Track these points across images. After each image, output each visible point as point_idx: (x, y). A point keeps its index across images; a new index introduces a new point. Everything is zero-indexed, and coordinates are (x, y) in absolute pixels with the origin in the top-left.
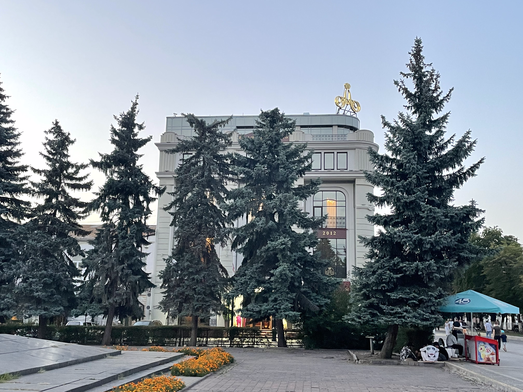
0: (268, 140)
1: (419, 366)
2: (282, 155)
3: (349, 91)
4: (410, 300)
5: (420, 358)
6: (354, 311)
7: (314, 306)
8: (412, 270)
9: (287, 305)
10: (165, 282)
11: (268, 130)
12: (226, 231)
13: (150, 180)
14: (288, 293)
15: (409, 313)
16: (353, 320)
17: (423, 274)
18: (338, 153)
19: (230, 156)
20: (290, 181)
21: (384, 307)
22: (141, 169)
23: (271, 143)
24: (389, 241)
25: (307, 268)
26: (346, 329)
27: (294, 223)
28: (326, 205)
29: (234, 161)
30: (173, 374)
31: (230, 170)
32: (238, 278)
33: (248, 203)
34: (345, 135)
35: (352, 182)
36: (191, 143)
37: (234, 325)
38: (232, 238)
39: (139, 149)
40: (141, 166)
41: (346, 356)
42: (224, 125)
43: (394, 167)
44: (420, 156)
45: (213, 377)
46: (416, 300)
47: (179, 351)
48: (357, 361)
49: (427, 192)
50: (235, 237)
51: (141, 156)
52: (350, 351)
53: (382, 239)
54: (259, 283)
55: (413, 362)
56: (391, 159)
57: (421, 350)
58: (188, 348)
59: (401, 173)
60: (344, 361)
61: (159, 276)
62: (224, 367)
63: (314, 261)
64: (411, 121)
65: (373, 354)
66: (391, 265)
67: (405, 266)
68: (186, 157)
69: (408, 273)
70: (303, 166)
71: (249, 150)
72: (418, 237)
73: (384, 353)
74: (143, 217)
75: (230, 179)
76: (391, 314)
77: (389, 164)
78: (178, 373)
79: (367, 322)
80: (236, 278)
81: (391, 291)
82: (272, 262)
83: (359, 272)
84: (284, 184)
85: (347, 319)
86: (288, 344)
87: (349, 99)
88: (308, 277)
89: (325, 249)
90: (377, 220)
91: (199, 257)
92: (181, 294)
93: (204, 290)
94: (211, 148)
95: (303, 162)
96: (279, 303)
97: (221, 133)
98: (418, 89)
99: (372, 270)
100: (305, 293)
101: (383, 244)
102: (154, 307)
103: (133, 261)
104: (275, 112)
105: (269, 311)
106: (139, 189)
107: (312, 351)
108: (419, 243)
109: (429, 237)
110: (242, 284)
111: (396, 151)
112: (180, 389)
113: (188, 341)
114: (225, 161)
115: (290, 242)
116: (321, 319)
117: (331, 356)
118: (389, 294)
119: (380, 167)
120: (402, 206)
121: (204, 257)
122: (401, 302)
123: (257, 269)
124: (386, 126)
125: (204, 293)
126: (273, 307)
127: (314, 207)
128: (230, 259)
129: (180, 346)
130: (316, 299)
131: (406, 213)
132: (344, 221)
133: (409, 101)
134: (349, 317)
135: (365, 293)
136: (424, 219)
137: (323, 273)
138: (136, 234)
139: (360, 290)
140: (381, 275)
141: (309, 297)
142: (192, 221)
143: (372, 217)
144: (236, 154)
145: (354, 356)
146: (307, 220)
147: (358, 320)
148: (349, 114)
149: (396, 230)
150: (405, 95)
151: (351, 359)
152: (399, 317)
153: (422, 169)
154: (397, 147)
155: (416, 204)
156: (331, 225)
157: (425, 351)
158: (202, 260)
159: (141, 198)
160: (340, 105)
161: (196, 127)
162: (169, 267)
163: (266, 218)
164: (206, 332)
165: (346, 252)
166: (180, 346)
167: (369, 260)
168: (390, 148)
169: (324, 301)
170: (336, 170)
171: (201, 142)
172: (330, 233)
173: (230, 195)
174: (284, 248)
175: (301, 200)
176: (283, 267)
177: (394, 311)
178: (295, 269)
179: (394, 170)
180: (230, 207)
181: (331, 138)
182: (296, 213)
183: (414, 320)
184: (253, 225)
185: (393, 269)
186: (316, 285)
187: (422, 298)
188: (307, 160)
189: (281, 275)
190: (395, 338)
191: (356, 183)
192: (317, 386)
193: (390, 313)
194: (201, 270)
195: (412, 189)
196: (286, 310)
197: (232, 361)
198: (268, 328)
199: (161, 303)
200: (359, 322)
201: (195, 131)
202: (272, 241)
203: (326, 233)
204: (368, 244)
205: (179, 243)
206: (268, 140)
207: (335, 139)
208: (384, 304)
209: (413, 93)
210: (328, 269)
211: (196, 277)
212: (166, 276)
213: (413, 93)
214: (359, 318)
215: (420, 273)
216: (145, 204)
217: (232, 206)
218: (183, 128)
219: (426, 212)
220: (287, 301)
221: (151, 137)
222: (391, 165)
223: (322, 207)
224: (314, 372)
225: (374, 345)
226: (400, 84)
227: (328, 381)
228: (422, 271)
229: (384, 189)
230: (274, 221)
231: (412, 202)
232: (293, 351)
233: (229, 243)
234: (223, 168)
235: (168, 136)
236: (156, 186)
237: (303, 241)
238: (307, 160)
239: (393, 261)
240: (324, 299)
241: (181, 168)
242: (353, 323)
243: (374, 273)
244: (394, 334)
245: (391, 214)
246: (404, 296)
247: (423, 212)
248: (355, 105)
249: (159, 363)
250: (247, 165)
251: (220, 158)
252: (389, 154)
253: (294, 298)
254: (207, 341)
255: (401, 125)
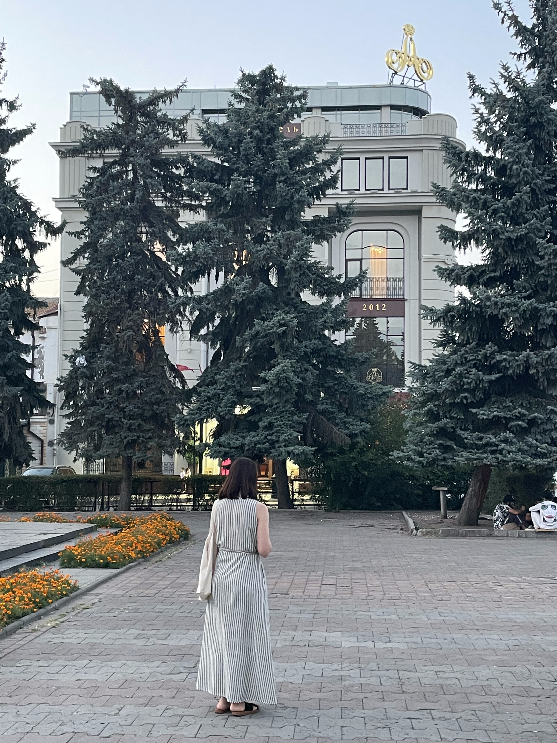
0: (254, 128)
1: (526, 537)
2: (282, 157)
3: (411, 39)
4: (513, 420)
5: (530, 523)
6: (411, 442)
7: (340, 435)
8: (519, 366)
9: (291, 435)
10: (68, 397)
11: (254, 108)
12: (178, 301)
13: (33, 209)
14: (293, 414)
15: (511, 443)
16: (409, 459)
17: (538, 372)
18: (390, 158)
19: (182, 160)
20: (296, 206)
21: (465, 434)
22: (16, 187)
23: (260, 134)
24: (476, 312)
25: (329, 368)
26: (395, 474)
27: (305, 287)
28: (366, 255)
29: (190, 170)
30: (64, 565)
31: (185, 188)
32: (203, 389)
33: (218, 249)
34: (404, 125)
35: (416, 212)
36: (107, 136)
37: (203, 473)
38: (191, 315)
39: (11, 149)
40: (15, 181)
41: (397, 523)
42: (171, 100)
43: (491, 173)
44: (538, 149)
45: (142, 567)
46: (523, 421)
47: (90, 521)
48: (415, 532)
49: (549, 219)
50: (197, 313)
51: (15, 162)
52: (404, 513)
53: (464, 309)
54: (241, 398)
55: (517, 532)
56: (485, 158)
57: (530, 509)
58: (104, 515)
59: (503, 182)
60: (392, 532)
61: (57, 385)
62: (168, 548)
63: (342, 355)
64: (523, 81)
65: (446, 517)
66: (480, 357)
67: (505, 360)
68: (99, 164)
69: (511, 371)
70: (322, 179)
71: (220, 149)
72: (531, 304)
73: (464, 517)
74: (25, 278)
75: (186, 207)
76: (478, 447)
77: (480, 169)
78: (73, 563)
79: (435, 460)
80: (199, 389)
81: (480, 404)
82: (264, 357)
83: (422, 373)
84: (286, 214)
85: (399, 458)
86: (296, 503)
87: (412, 54)
88: (331, 384)
89: (369, 336)
90: (454, 275)
91: (131, 352)
92: (98, 418)
93: (140, 411)
94: (147, 144)
95: (322, 172)
96: (277, 432)
97: (165, 115)
98: (538, 19)
99: (445, 367)
100: (324, 412)
101: (466, 319)
102: (52, 444)
103: (6, 360)
104: (268, 73)
105: (258, 446)
106: (13, 226)
107: (337, 515)
108: (534, 316)
109: (552, 304)
110: (209, 399)
111: (494, 141)
112: (66, 595)
113: (116, 502)
114: (174, 170)
115: (295, 321)
116: (353, 458)
117: (370, 522)
118: (474, 411)
119: (462, 175)
120: (503, 248)
121: (139, 351)
122: (496, 424)
123: (236, 371)
124: (476, 95)
125: (141, 416)
126: (266, 438)
127: (347, 261)
128: (187, 352)
129: (102, 509)
130: (345, 423)
131: (509, 260)
132: (401, 284)
133: (522, 41)
134: (401, 454)
135: (430, 410)
136: (543, 271)
137: (361, 378)
138: (10, 310)
139: (423, 404)
140: (461, 376)
141: (331, 418)
142: (114, 285)
143: (446, 270)
144: (195, 157)
145: (411, 522)
146: (331, 281)
147: (418, 459)
148: (411, 84)
149: (491, 293)
150: (513, 30)
151: (405, 529)
152: (493, 452)
153: (543, 175)
154: (495, 132)
155: (528, 243)
156: (378, 292)
157: (539, 512)
158: (138, 357)
159: (19, 243)
160: (395, 66)
161: (117, 104)
162: (75, 369)
163: (254, 277)
164: (149, 484)
165: (403, 339)
166: (102, 509)
167: (440, 350)
168: (482, 136)
169: (358, 427)
170: (386, 190)
171: (127, 133)
172: (375, 307)
173: (186, 236)
174: (284, 332)
175: (317, 243)
176: (283, 365)
177: (484, 441)
178: (307, 370)
179: (490, 178)
180: (185, 257)
181: (378, 130)
182: (309, 267)
183: (519, 457)
184: (227, 290)
185: (483, 365)
186: (344, 399)
187: (535, 417)
188: (329, 168)
189: (279, 381)
190: (485, 489)
191: (424, 215)
192: (332, 581)
193: (476, 445)
194: (135, 374)
195: (522, 214)
196: (288, 443)
197: (185, 536)
198: (266, 476)
199: (62, 435)
200: (420, 462)
201: (116, 112)
202: (263, 319)
203: (368, 308)
204: (438, 320)
205: (91, 325)
206: (254, 128)
207: (385, 132)
208: (465, 430)
209: (530, 27)
210: (371, 371)
211: (124, 387)
212: (68, 386)
213: (530, 27)
214: (421, 454)
215: (532, 372)
216: (27, 254)
217: (189, 254)
218: (102, 113)
219: (546, 258)
220: (291, 428)
221: (34, 125)
222: (485, 169)
223: (361, 260)
224: (332, 554)
225: (447, 501)
226: (505, 8)
227: (354, 569)
228: (536, 368)
229: (470, 214)
230: (269, 283)
231: (519, 239)
232: (305, 515)
233: (186, 327)
234: (171, 183)
235: (73, 129)
236: (46, 220)
237: (322, 320)
238: (329, 168)
239: (483, 351)
240: (359, 423)
241: (91, 184)
242: (410, 464)
243: (448, 372)
244: (484, 483)
245: (482, 263)
246: (502, 414)
247: (542, 257)
248: (422, 68)
249: (42, 544)
250: (216, 177)
251: (165, 164)
252: (482, 148)
253: (305, 421)
254: (151, 501)
255: (504, 88)
